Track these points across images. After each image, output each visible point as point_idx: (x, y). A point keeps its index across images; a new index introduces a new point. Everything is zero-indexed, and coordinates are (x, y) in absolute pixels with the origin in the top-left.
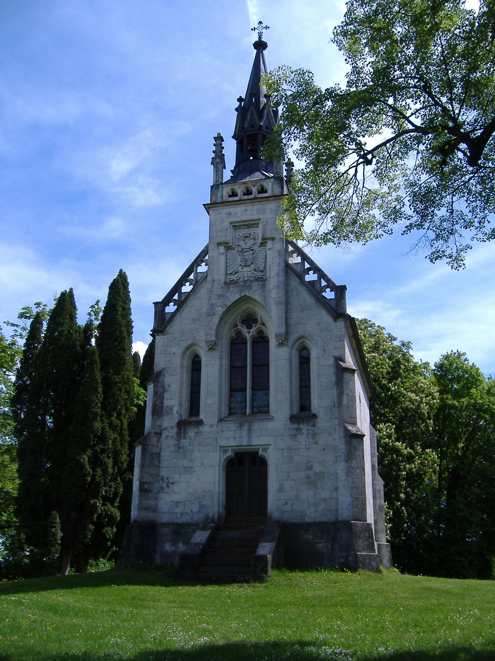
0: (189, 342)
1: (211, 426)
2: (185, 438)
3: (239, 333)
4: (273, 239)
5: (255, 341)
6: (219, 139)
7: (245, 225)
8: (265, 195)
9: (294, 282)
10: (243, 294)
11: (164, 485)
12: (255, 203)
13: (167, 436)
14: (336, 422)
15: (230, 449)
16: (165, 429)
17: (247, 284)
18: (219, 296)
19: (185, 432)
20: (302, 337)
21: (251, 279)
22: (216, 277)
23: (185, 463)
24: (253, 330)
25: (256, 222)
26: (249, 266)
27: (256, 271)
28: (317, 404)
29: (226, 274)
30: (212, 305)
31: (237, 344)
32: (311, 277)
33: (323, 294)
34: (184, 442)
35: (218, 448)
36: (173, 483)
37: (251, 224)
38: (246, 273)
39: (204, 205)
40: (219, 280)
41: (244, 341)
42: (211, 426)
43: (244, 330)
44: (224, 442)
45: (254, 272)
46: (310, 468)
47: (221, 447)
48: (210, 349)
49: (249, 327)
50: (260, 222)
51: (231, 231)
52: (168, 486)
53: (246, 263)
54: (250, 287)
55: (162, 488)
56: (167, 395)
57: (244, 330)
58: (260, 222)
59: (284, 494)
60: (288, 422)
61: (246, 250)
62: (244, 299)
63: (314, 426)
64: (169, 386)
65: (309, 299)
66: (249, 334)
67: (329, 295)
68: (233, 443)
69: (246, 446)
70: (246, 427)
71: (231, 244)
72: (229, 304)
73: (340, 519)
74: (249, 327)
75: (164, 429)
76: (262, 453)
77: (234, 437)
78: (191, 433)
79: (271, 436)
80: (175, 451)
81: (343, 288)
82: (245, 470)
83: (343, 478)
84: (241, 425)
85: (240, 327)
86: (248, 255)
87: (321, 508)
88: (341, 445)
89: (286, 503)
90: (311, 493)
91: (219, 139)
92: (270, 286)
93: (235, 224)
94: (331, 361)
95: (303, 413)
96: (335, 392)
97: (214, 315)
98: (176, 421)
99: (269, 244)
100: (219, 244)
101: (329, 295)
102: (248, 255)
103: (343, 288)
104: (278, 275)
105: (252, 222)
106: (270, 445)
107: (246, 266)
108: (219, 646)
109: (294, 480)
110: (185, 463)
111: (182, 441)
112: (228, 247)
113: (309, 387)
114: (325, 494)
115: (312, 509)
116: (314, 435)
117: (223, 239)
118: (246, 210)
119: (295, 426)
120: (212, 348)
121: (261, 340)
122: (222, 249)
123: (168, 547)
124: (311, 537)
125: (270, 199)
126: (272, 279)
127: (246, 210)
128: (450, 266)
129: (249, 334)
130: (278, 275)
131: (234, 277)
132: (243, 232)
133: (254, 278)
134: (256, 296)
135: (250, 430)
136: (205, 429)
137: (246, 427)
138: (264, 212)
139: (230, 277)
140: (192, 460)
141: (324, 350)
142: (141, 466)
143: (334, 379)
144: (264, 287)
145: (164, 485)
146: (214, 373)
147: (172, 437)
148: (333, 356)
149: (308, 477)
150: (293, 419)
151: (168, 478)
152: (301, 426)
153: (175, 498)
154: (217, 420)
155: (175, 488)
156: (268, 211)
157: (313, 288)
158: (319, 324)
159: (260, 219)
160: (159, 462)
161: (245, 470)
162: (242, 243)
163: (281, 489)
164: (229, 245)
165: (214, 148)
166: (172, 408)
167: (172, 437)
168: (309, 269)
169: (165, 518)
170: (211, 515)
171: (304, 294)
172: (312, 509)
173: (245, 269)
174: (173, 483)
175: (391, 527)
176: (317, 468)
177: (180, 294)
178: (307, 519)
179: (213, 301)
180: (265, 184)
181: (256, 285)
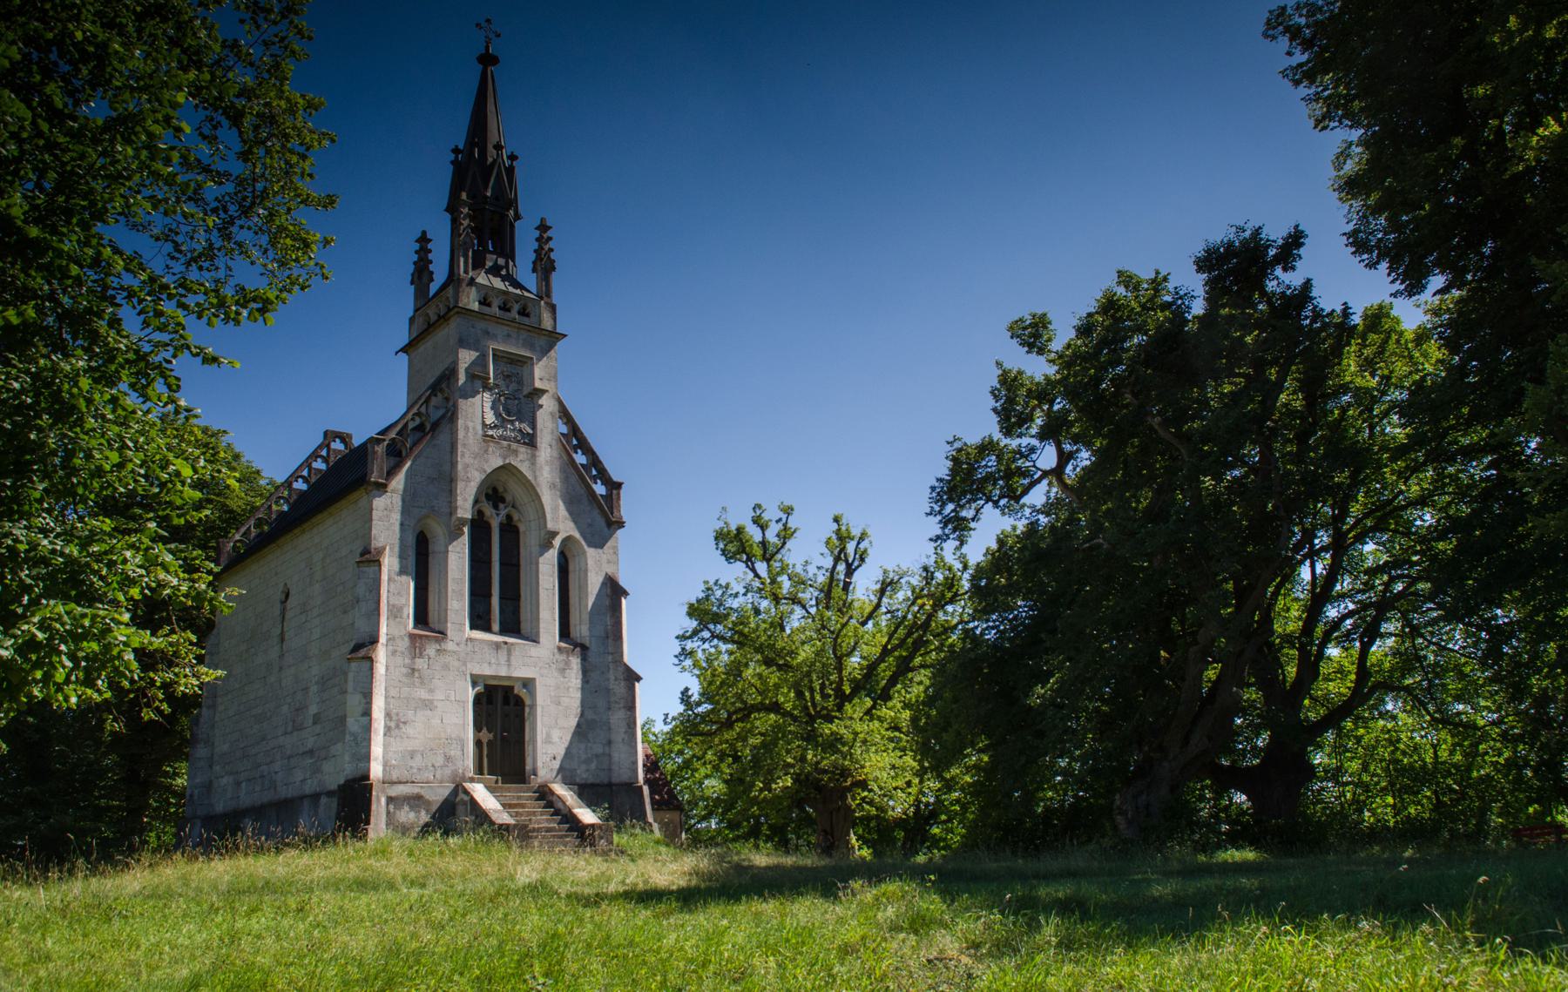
2: (421, 656)
3: (480, 513)
5: (503, 527)
6: (424, 239)
19: (422, 650)
23: (422, 694)
34: (420, 663)
41: (488, 527)
43: (488, 510)
52: (397, 726)
54: (516, 452)
62: (507, 469)
67: (600, 489)
68: (488, 671)
73: (615, 780)
78: (431, 650)
80: (407, 675)
81: (619, 486)
90: (582, 746)
91: (424, 239)
101: (600, 489)
103: (619, 486)
110: (422, 694)
113: (473, 593)
114: (598, 749)
115: (584, 767)
128: (939, 532)
140: (431, 691)
155: (408, 730)
158: (590, 525)
165: (430, 256)
172: (584, 767)
175: (987, 771)
177: (594, 479)
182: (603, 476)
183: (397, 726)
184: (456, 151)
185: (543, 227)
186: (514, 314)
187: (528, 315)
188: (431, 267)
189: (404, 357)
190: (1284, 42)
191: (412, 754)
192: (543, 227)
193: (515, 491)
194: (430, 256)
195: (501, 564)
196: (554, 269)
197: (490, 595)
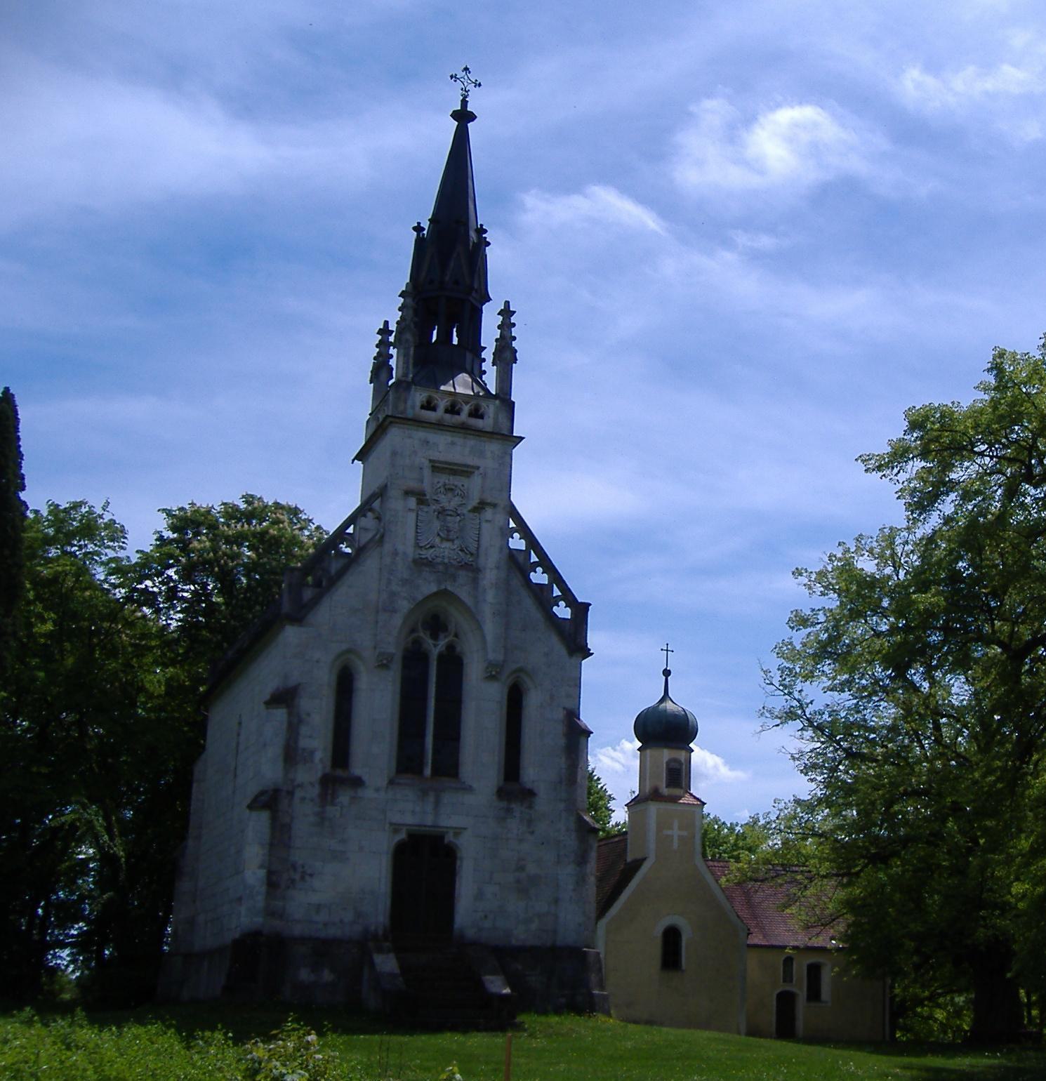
0: (344, 647)
1: (377, 790)
2: (333, 804)
3: (417, 642)
4: (494, 506)
7: (451, 469)
8: (479, 423)
9: (516, 581)
10: (443, 587)
11: (297, 877)
12: (469, 436)
13: (303, 799)
14: (562, 806)
15: (404, 829)
16: (301, 786)
17: (448, 570)
18: (405, 582)
20: (521, 670)
21: (454, 563)
22: (400, 548)
24: (442, 643)
25: (469, 470)
26: (452, 541)
27: (462, 550)
28: (531, 772)
29: (417, 546)
30: (393, 595)
31: (414, 659)
32: (539, 577)
33: (555, 609)
34: (332, 811)
35: (387, 826)
36: (311, 875)
37: (465, 471)
38: (447, 550)
39: (524, 438)
40: (405, 553)
42: (377, 790)
43: (429, 642)
44: (397, 818)
45: (460, 552)
46: (521, 868)
47: (391, 824)
48: (379, 666)
49: (435, 636)
50: (476, 472)
51: (427, 472)
52: (302, 878)
53: (448, 535)
54: (454, 578)
55: (293, 881)
56: (304, 730)
57: (429, 642)
58: (476, 472)
59: (480, 900)
60: (495, 797)
61: (450, 513)
62: (443, 594)
63: (530, 807)
64: (309, 715)
65: (537, 615)
66: (435, 648)
67: (563, 611)
68: (409, 819)
69: (429, 826)
70: (431, 798)
71: (428, 497)
72: (420, 598)
74: (435, 636)
75: (299, 786)
76: (452, 839)
77: (410, 810)
78: (344, 797)
79: (467, 814)
82: (424, 864)
83: (571, 887)
84: (425, 793)
85: (422, 634)
86: (453, 522)
87: (534, 926)
88: (571, 841)
89: (486, 917)
92: (485, 582)
93: (437, 465)
94: (560, 714)
95: (512, 786)
96: (562, 762)
97: (394, 611)
98: (319, 774)
99: (488, 514)
100: (408, 493)
101: (563, 611)
102: (453, 522)
104: (498, 568)
105: (465, 469)
106: (465, 829)
107: (448, 540)
108: (142, 1022)
109: (499, 884)
111: (329, 808)
112: (422, 499)
116: (530, 822)
117: (413, 484)
118: (453, 443)
119: (504, 804)
120: (383, 664)
121: (453, 664)
122: (412, 502)
123: (305, 975)
124: (520, 967)
125: (495, 436)
126: (488, 571)
127: (453, 443)
129: (435, 648)
130: (498, 568)
131: (428, 554)
132: (444, 479)
133: (459, 562)
134: (464, 593)
135: (437, 803)
136: (368, 793)
137: (431, 798)
138: (482, 454)
139: (421, 553)
141: (552, 697)
142: (271, 845)
143: (562, 741)
144: (475, 582)
145: (297, 877)
146: (378, 702)
147: (312, 800)
148: (564, 708)
149: (518, 881)
150: (502, 793)
151: (303, 867)
152: (513, 806)
153: (315, 898)
154: (386, 782)
156: (489, 454)
157: (542, 597)
159: (478, 468)
160: (290, 838)
161: (424, 864)
162: (442, 498)
163: (480, 896)
164: (425, 498)
166: (312, 753)
167: (312, 800)
168: (536, 564)
169: (297, 930)
170: (373, 928)
171: (529, 603)
173: (448, 545)
174: (311, 875)
176: (532, 869)
178: (514, 942)
179: (394, 588)
180: (483, 404)
181: (463, 576)
182: (568, 597)
183: (302, 878)
184: (418, 229)
185: (507, 312)
186: (463, 417)
187: (482, 417)
188: (21, 449)
189: (358, 463)
190: (809, 733)
191: (319, 907)
192: (507, 312)
193: (456, 618)
194: (513, 320)
195: (437, 700)
196: (515, 360)
197: (422, 736)
